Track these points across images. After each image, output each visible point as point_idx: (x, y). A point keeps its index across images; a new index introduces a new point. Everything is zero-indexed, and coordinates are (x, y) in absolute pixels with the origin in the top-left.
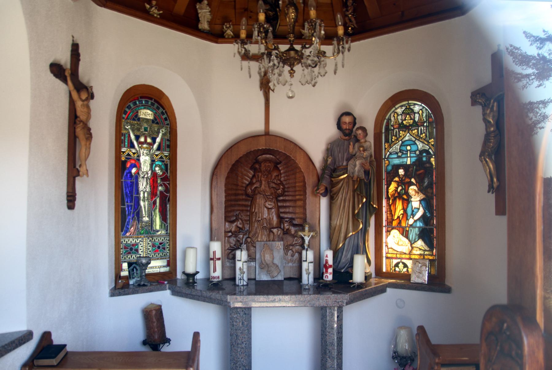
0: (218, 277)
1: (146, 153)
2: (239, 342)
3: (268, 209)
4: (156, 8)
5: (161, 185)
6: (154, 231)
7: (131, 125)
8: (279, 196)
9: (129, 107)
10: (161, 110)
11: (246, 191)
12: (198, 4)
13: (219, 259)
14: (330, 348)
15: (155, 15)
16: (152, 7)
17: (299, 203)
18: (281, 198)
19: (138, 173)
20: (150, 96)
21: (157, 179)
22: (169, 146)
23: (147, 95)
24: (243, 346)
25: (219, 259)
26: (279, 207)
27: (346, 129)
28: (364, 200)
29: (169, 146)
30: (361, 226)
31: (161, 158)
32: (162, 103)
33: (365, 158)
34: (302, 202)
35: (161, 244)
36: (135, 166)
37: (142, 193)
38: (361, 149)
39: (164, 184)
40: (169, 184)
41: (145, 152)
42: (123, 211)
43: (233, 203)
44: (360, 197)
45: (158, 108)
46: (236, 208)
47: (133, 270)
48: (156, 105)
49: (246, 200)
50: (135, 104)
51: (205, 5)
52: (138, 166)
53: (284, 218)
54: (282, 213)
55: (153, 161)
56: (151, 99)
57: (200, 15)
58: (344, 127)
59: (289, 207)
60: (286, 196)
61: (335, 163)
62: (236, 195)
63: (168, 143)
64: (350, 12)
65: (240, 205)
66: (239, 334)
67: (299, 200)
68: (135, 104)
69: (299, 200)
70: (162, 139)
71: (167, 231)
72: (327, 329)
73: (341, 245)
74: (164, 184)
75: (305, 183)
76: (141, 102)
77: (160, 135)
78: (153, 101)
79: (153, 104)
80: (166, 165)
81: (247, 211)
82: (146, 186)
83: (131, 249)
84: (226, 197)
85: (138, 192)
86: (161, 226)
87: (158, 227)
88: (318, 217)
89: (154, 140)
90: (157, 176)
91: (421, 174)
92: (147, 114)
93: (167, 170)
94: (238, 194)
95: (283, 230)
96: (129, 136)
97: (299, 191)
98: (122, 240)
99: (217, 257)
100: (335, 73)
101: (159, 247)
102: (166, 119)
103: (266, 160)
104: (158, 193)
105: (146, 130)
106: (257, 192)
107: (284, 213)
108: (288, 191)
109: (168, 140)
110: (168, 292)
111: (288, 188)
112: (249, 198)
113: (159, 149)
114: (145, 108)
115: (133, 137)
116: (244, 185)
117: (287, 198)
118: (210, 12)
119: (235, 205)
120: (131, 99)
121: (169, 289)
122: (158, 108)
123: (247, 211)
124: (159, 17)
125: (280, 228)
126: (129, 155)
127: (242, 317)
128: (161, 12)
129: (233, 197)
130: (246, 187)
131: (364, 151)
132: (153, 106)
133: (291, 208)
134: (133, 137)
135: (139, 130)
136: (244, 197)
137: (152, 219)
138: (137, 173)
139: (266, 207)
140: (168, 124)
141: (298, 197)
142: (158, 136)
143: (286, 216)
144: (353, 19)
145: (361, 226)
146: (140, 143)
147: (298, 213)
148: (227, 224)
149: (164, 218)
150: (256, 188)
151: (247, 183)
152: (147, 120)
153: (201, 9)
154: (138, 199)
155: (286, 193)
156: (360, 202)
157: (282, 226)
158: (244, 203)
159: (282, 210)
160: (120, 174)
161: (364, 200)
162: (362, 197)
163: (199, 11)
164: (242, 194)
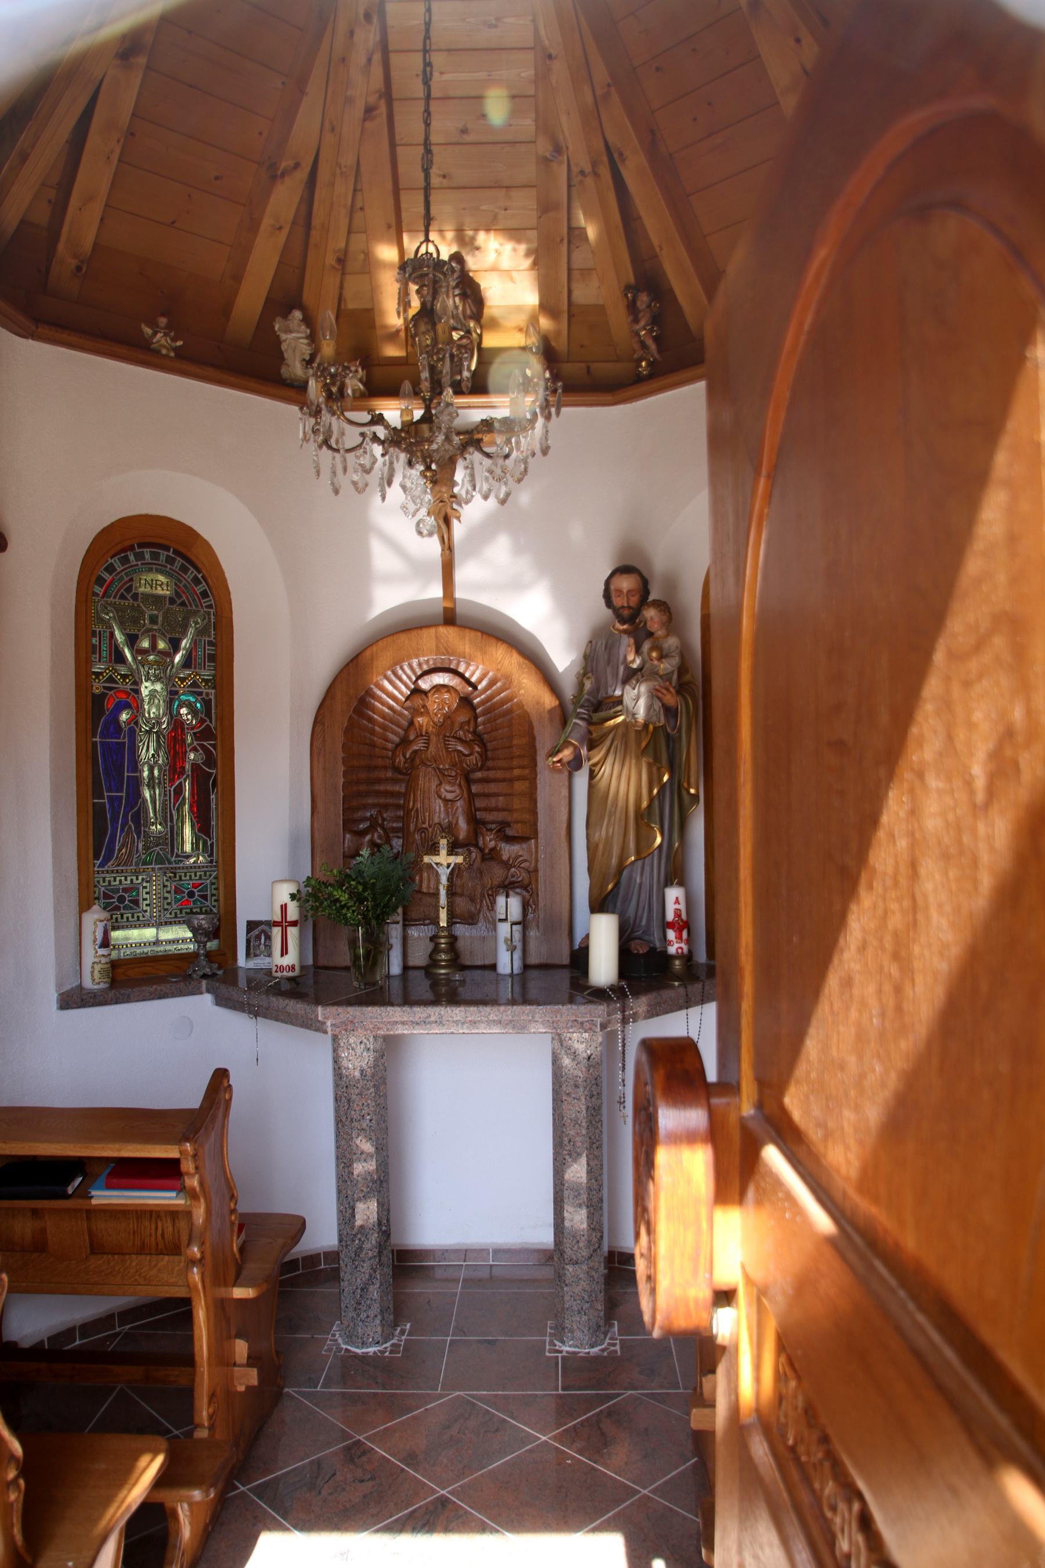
0: (293, 967)
1: (155, 676)
2: (355, 1115)
3: (446, 801)
4: (166, 335)
5: (194, 749)
6: (177, 856)
7: (118, 609)
8: (473, 771)
9: (110, 569)
10: (192, 572)
11: (393, 758)
12: (279, 319)
13: (294, 924)
14: (572, 1133)
15: (164, 352)
16: (155, 333)
17: (520, 786)
18: (479, 775)
19: (137, 723)
20: (161, 541)
21: (183, 733)
22: (212, 658)
23: (155, 540)
24: (364, 1126)
25: (294, 924)
26: (471, 797)
27: (623, 607)
28: (666, 778)
29: (212, 658)
30: (659, 840)
31: (195, 684)
32: (194, 559)
33: (667, 677)
34: (527, 784)
35: (195, 886)
36: (126, 706)
37: (146, 769)
38: (654, 654)
39: (203, 747)
40: (214, 746)
41: (152, 672)
42: (99, 812)
43: (363, 788)
44: (654, 769)
45: (184, 569)
46: (370, 801)
47: (258, 937)
48: (179, 561)
49: (395, 781)
50: (125, 560)
51: (296, 322)
52: (134, 705)
53: (484, 823)
54: (479, 810)
55: (172, 695)
56: (166, 548)
57: (284, 347)
58: (618, 602)
59: (496, 795)
60: (489, 769)
61: (598, 690)
62: (370, 768)
63: (210, 650)
64: (642, 323)
65: (378, 794)
66: (354, 1097)
67: (519, 778)
68: (125, 560)
69: (519, 778)
70: (195, 643)
71: (211, 855)
72: (564, 1088)
73: (610, 887)
74: (203, 747)
75: (533, 739)
76: (140, 557)
77: (191, 631)
78: (171, 554)
79: (170, 561)
80: (207, 703)
81: (398, 807)
82: (156, 751)
83: (122, 899)
84: (345, 774)
85: (135, 766)
86: (195, 846)
87: (188, 848)
88: (564, 818)
89: (175, 645)
90: (183, 729)
91: (618, 726)
92: (157, 584)
93: (208, 714)
94: (376, 768)
95: (482, 850)
96: (112, 635)
97: (520, 756)
98: (99, 878)
99: (289, 919)
100: (336, 492)
101: (191, 894)
102: (205, 595)
103: (438, 688)
104: (188, 767)
105: (153, 620)
106: (418, 761)
107: (485, 809)
108: (493, 759)
109: (210, 643)
110: (208, 998)
111: (495, 749)
112: (401, 777)
113: (187, 663)
114: (150, 570)
115: (119, 636)
116: (390, 746)
117: (492, 774)
118: (307, 338)
119: (368, 794)
120: (113, 551)
121: (208, 991)
122: (184, 569)
123: (398, 807)
124: (172, 354)
125: (476, 846)
126: (111, 680)
127: (361, 1055)
128: (180, 343)
129: (363, 775)
130: (394, 751)
131: (661, 658)
132: (172, 564)
133: (501, 798)
134: (119, 636)
135: (135, 621)
136: (389, 774)
137: (172, 828)
138: (134, 720)
139: (440, 797)
140: (210, 606)
141: (517, 772)
142: (184, 634)
143: (490, 817)
144: (651, 343)
145: (659, 840)
146: (138, 652)
147: (516, 810)
148: (348, 836)
149: (203, 827)
150: (416, 752)
151: (397, 739)
152: (157, 600)
153: (288, 331)
154: (136, 784)
155: (490, 764)
156: (655, 783)
157: (481, 843)
158: (389, 787)
159: (479, 803)
160: (90, 727)
161: (666, 778)
162: (659, 769)
163: (283, 336)
164: (385, 768)
